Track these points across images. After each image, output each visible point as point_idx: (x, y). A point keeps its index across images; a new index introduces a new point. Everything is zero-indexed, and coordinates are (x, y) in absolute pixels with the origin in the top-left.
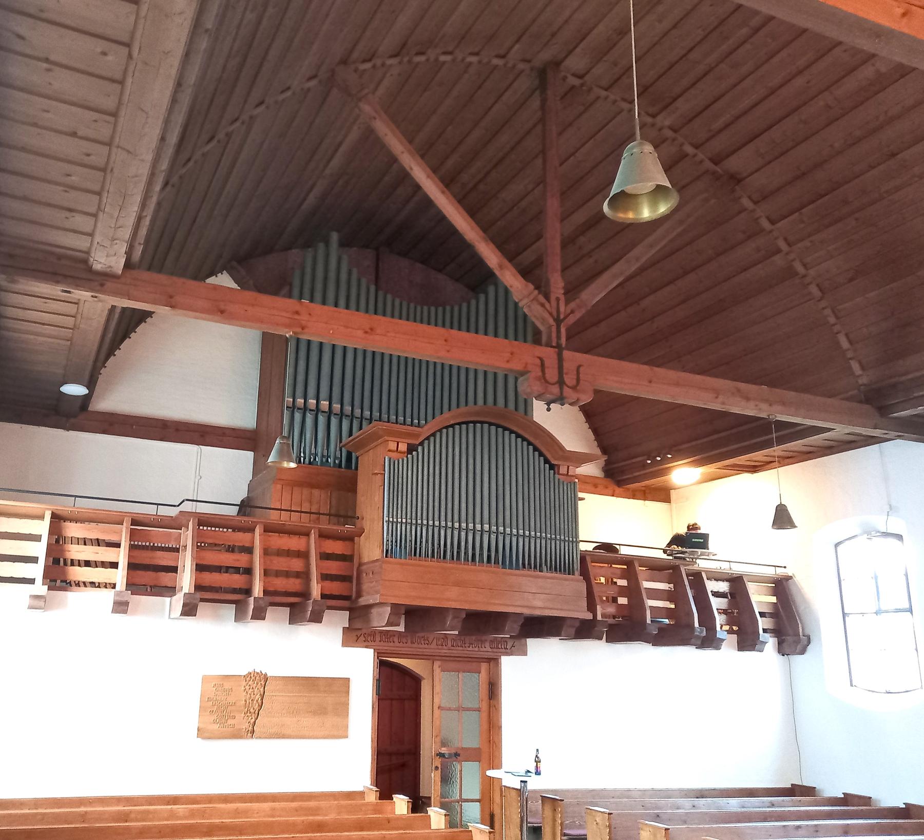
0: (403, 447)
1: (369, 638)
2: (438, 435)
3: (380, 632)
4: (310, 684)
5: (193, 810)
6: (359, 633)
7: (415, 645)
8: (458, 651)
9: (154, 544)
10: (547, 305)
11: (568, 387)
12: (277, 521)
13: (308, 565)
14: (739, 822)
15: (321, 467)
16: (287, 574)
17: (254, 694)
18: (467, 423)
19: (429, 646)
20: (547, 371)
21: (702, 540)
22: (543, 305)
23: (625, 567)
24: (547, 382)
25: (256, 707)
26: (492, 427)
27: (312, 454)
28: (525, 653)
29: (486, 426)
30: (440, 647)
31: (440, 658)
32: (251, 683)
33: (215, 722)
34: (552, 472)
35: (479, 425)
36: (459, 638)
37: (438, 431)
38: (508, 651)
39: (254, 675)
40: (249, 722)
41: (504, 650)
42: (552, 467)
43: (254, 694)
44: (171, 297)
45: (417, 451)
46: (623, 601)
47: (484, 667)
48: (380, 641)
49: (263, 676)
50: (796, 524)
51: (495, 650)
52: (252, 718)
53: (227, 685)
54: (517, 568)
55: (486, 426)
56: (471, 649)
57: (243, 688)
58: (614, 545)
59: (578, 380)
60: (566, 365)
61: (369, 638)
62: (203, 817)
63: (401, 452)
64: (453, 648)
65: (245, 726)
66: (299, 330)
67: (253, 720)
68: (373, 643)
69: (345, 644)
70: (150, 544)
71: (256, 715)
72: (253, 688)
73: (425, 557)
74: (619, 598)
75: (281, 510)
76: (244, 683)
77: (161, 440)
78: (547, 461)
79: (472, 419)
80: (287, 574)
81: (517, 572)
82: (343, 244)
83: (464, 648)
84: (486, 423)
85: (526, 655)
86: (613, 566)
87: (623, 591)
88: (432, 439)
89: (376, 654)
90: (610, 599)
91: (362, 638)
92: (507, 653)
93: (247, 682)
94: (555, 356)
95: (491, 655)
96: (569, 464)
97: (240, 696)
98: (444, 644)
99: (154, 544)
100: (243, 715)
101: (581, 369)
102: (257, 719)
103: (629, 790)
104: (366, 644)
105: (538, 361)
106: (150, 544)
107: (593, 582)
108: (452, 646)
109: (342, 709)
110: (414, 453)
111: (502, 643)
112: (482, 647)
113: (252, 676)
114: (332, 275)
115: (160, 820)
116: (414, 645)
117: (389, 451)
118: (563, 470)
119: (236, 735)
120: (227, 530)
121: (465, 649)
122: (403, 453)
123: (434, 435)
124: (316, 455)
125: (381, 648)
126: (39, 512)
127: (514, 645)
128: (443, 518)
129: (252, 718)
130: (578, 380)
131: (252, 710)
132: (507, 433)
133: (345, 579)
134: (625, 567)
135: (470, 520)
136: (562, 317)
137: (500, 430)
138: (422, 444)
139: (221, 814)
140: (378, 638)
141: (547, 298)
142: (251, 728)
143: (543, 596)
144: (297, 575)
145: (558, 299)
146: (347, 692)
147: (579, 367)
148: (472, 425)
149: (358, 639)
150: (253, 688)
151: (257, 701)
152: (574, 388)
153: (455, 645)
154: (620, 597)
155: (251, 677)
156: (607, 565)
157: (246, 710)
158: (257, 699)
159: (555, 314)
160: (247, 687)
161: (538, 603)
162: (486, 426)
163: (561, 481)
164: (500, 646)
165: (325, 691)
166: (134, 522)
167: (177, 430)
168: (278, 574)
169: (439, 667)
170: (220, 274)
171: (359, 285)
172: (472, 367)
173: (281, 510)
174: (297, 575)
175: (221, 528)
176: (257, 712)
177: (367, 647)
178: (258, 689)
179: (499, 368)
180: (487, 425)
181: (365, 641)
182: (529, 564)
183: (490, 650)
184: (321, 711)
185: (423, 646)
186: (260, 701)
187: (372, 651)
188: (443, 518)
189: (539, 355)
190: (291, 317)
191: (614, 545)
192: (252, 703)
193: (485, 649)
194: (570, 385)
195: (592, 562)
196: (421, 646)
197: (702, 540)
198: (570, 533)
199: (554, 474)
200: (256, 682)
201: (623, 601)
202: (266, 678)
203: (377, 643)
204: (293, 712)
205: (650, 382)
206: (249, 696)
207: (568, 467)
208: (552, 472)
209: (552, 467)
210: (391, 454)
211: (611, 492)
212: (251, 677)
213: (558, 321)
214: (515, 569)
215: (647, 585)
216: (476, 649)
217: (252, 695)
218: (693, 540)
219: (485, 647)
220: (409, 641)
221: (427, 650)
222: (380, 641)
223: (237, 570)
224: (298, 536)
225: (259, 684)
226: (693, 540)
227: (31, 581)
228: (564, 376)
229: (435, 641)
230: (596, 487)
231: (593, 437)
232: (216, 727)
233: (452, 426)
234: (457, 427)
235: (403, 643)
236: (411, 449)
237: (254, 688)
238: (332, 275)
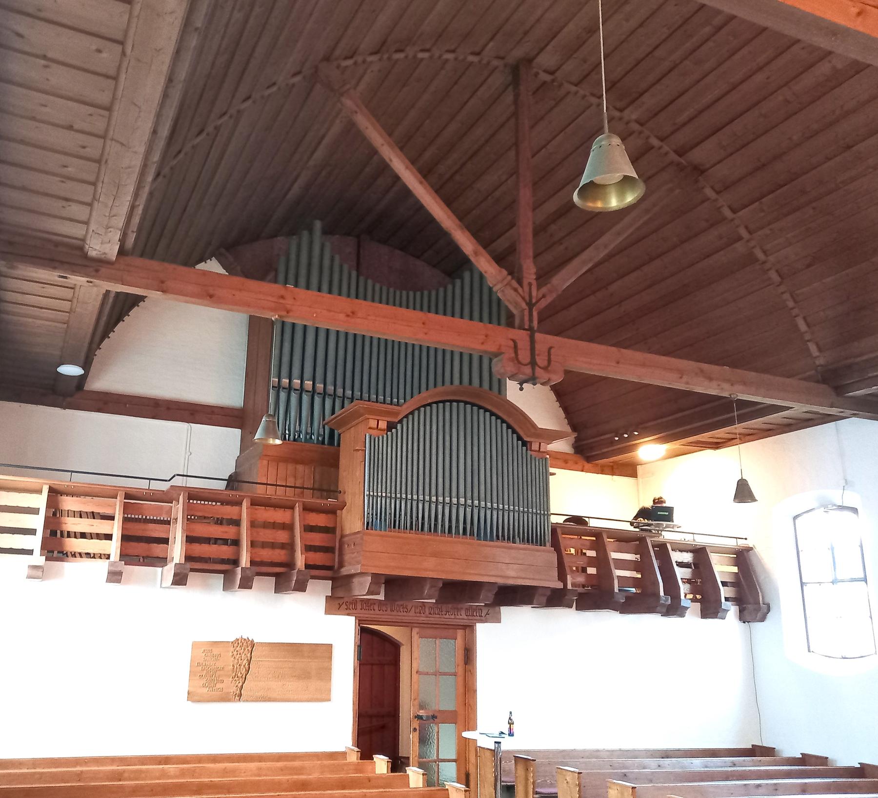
0: (383, 425)
1: (351, 606)
2: (416, 413)
3: (361, 601)
4: (295, 649)
5: (183, 769)
6: (341, 601)
7: (395, 613)
8: (435, 619)
9: (146, 517)
10: (520, 290)
11: (540, 367)
12: (263, 494)
13: (292, 537)
14: (702, 781)
15: (305, 444)
16: (273, 546)
17: (241, 660)
18: (444, 402)
19: (408, 614)
20: (519, 352)
21: (667, 513)
22: (516, 290)
23: (594, 539)
24: (519, 363)
25: (244, 671)
26: (467, 405)
27: (297, 431)
28: (498, 621)
29: (462, 405)
30: (418, 615)
31: (418, 625)
32: (238, 649)
33: (204, 686)
34: (524, 448)
35: (455, 404)
36: (436, 606)
37: (416, 409)
38: (483, 618)
39: (241, 642)
40: (236, 686)
41: (479, 617)
42: (525, 444)
43: (241, 660)
44: (163, 282)
45: (396, 428)
46: (592, 571)
47: (460, 633)
48: (361, 609)
49: (250, 642)
50: (757, 498)
51: (470, 618)
52: (239, 682)
53: (216, 651)
54: (492, 540)
55: (462, 405)
56: (447, 616)
57: (231, 654)
58: (583, 518)
59: (549, 361)
60: (538, 347)
61: (351, 606)
62: (193, 777)
63: (381, 430)
64: (430, 615)
65: (233, 689)
66: (284, 313)
67: (241, 684)
68: (354, 611)
69: (328, 611)
70: (142, 516)
71: (244, 679)
72: (240, 654)
73: (404, 529)
74: (588, 568)
75: (267, 484)
76: (232, 649)
77: (153, 418)
78: (519, 438)
79: (448, 398)
80: (273, 546)
81: (492, 543)
82: (326, 232)
83: (441, 616)
84: (462, 401)
85: (500, 622)
86: (583, 537)
87: (592, 562)
88: (410, 417)
89: (357, 621)
90: (580, 569)
91: (344, 606)
92: (481, 620)
93: (235, 648)
94: (528, 339)
95: (466, 622)
96: (540, 441)
97: (228, 661)
98: (422, 612)
99: (146, 517)
100: (231, 679)
101: (552, 351)
102: (244, 683)
103: (598, 751)
104: (348, 611)
105: (511, 343)
106: (142, 516)
107: (564, 553)
108: (429, 614)
109: (325, 673)
110: (394, 430)
111: (477, 610)
112: (458, 615)
113: (239, 642)
114: (316, 261)
115: (152, 779)
116: (393, 613)
117: (370, 428)
118: (535, 447)
119: (225, 698)
120: (216, 504)
121: (442, 616)
122: (383, 430)
123: (412, 413)
124: (300, 432)
125: (362, 615)
126: (37, 487)
127: (488, 613)
128: (421, 492)
129: (239, 682)
130: (549, 361)
131: (239, 675)
132: (482, 411)
133: (328, 550)
134: (594, 539)
135: (447, 494)
136: (534, 301)
137: (475, 408)
138: (401, 421)
139: (210, 773)
140: (359, 606)
141: (520, 283)
142: (238, 692)
143: (516, 566)
144: (283, 546)
145: (530, 284)
146: (330, 658)
147: (550, 348)
148: (449, 403)
149: (340, 607)
150: (240, 654)
151: (244, 666)
152: (545, 369)
153: (432, 613)
154: (589, 567)
155: (238, 643)
156: (576, 537)
157: (234, 674)
158: (244, 664)
159: (527, 298)
160: (235, 653)
161: (512, 573)
162: (462, 405)
163: (533, 457)
164: (475, 614)
165: (309, 657)
166: (128, 496)
167: (168, 409)
168: (264, 545)
169: (417, 634)
170: (209, 260)
171: (341, 271)
172: (448, 348)
173: (267, 484)
174: (283, 546)
175: (210, 501)
176: (244, 676)
177: (348, 615)
178: (245, 654)
179: (474, 349)
180: (463, 403)
181: (346, 609)
182: (503, 536)
183: (466, 617)
184: (305, 675)
185: (402, 614)
186: (247, 666)
187: (353, 618)
188: (421, 492)
189: (512, 338)
190: (276, 301)
191: (583, 518)
192: (240, 668)
193: (461, 617)
194: (542, 365)
195: (563, 534)
196: (400, 614)
197: (667, 513)
198: (542, 506)
199: (527, 450)
200: (243, 648)
201: (592, 571)
202: (253, 644)
203: (359, 611)
204: (279, 676)
205: (618, 363)
206: (236, 661)
207: (540, 443)
208: (524, 448)
209: (525, 444)
210: (372, 431)
211: (580, 467)
212: (238, 643)
213: (530, 305)
214: (490, 541)
215: (614, 555)
216: (453, 617)
217: (239, 661)
218: (659, 513)
219: (461, 615)
220: (389, 609)
221: (406, 618)
222: (361, 609)
223: (225, 542)
224: (283, 509)
225: (246, 650)
226: (659, 513)
227: (30, 552)
228: (536, 357)
229: (413, 608)
230: (566, 463)
231: (563, 415)
232: (205, 690)
233: (430, 405)
234: (434, 406)
235: (383, 611)
236: (391, 426)
237: (242, 653)
238: (316, 261)
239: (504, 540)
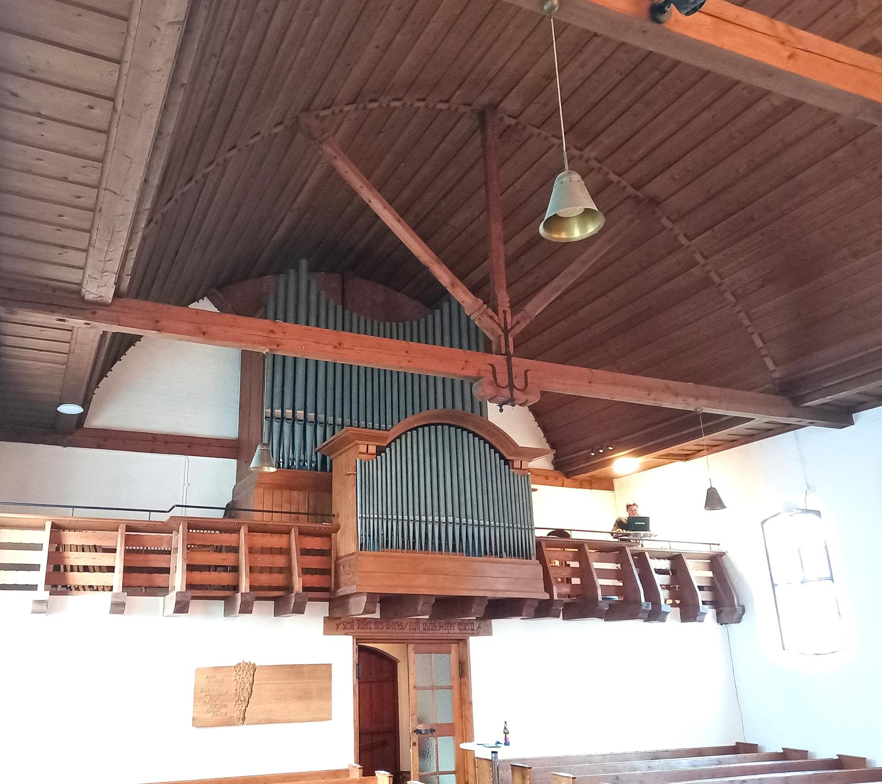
0: (372, 449)
3: (357, 620)
4: (295, 671)
8: (429, 634)
9: (147, 548)
16: (271, 570)
18: (429, 425)
21: (644, 523)
22: (491, 318)
24: (498, 386)
25: (246, 695)
40: (240, 710)
42: (507, 462)
43: (244, 683)
45: (385, 452)
51: (463, 632)
54: (480, 555)
56: (441, 631)
64: (425, 632)
65: (237, 714)
67: (244, 708)
68: (352, 631)
69: (327, 632)
70: (143, 548)
71: (247, 703)
75: (264, 511)
77: (152, 452)
80: (271, 570)
82: (312, 269)
85: (491, 635)
86: (566, 549)
90: (565, 580)
91: (341, 626)
106: (143, 548)
107: (549, 565)
109: (325, 693)
114: (303, 297)
117: (360, 453)
118: (517, 464)
119: (229, 723)
120: (215, 532)
123: (399, 437)
126: (40, 524)
131: (242, 698)
134: (577, 550)
136: (509, 328)
138: (389, 446)
140: (356, 627)
144: (280, 570)
150: (242, 678)
151: (247, 689)
152: (523, 390)
158: (246, 688)
160: (237, 677)
163: (516, 474)
165: (309, 677)
168: (262, 570)
169: (413, 649)
173: (264, 511)
174: (280, 570)
177: (346, 634)
179: (455, 374)
183: (459, 631)
184: (306, 696)
185: (397, 631)
192: (243, 692)
193: (455, 631)
196: (394, 631)
197: (644, 523)
199: (509, 468)
200: (245, 672)
201: (576, 581)
202: (254, 668)
208: (507, 467)
209: (507, 462)
213: (506, 331)
218: (636, 523)
220: (385, 627)
221: (402, 635)
226: (636, 523)
236: (380, 451)
238: (303, 297)
239: (492, 555)
